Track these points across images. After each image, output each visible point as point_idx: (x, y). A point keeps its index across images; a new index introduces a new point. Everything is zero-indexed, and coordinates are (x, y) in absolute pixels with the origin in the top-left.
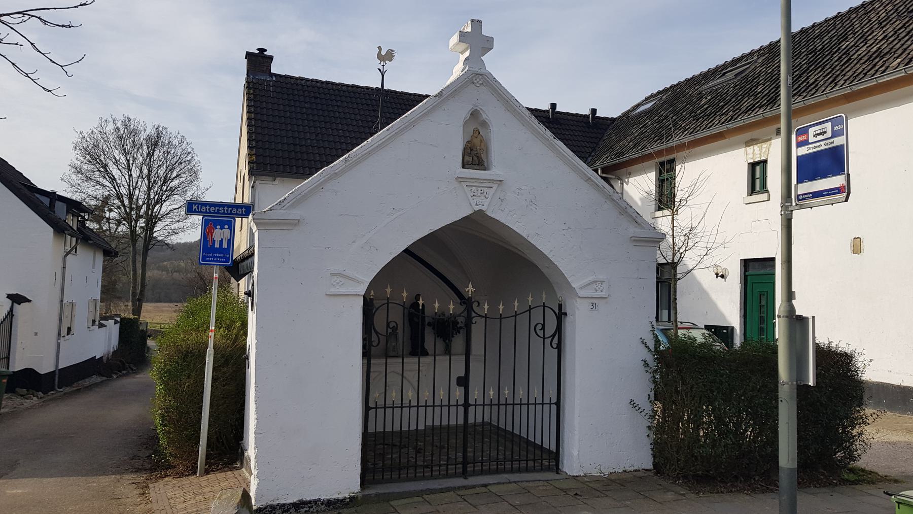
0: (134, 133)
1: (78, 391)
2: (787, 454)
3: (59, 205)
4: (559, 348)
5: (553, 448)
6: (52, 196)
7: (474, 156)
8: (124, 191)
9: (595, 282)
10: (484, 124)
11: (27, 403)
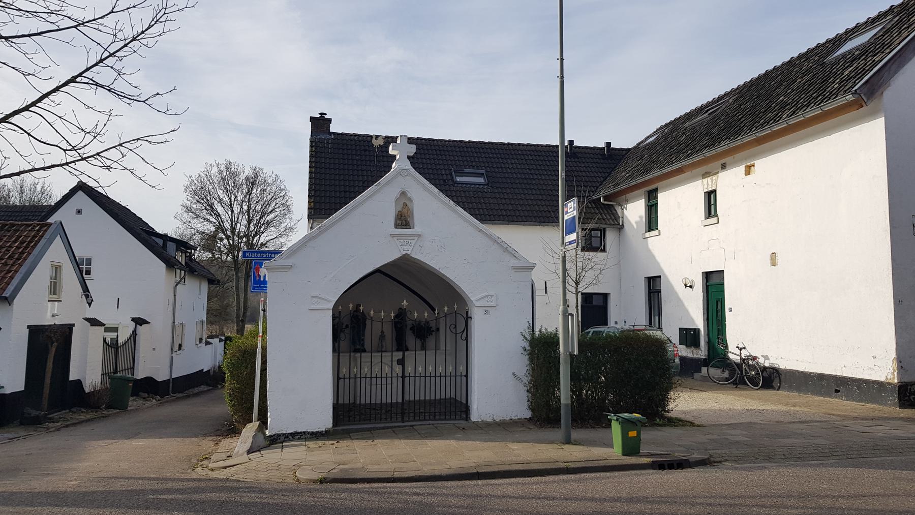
0: (234, 175)
1: (188, 396)
3: (170, 245)
6: (165, 238)
7: (403, 220)
8: (227, 225)
9: (487, 296)
10: (410, 200)
11: (148, 404)
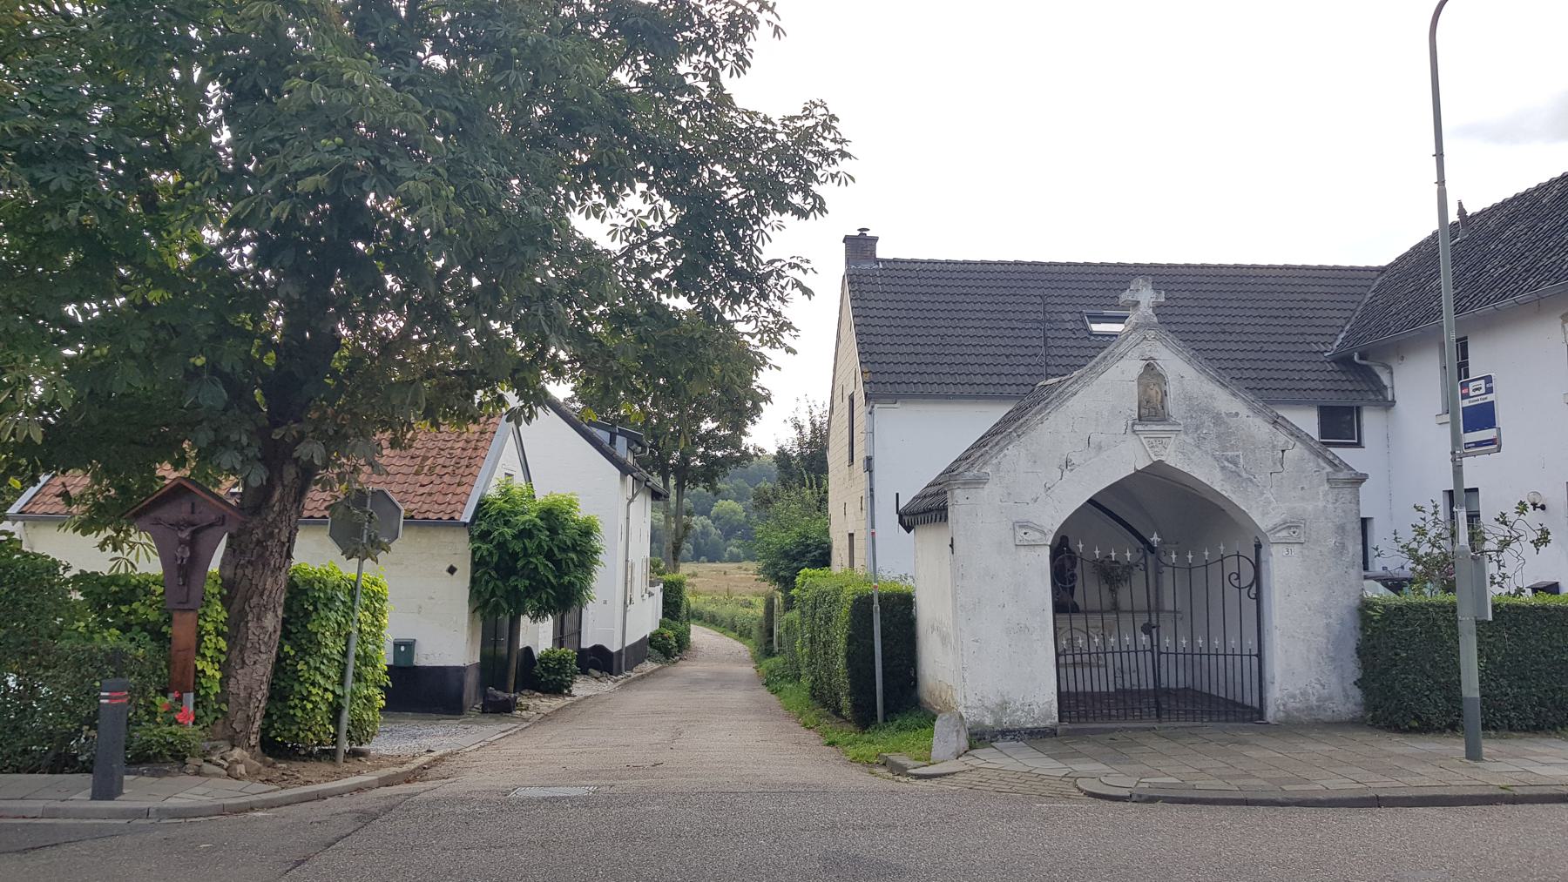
2: (1471, 686)
4: (1258, 598)
5: (1256, 704)
